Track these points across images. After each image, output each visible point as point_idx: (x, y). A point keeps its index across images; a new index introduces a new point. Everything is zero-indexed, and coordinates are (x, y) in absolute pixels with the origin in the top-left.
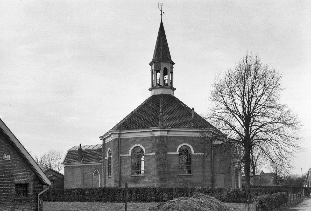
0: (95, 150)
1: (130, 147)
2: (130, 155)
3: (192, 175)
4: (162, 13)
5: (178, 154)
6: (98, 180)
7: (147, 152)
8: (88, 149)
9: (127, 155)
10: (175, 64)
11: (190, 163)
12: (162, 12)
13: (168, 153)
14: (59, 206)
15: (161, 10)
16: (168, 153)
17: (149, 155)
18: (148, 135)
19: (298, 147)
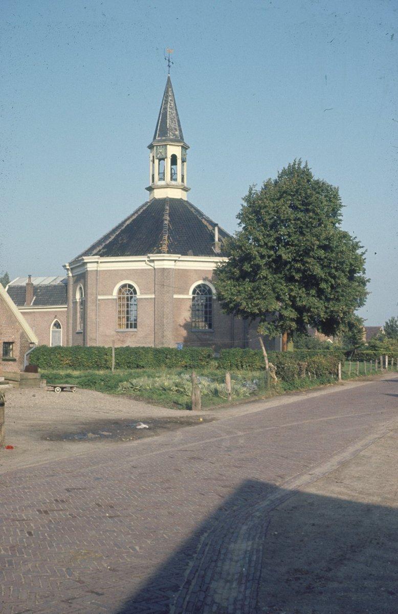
0: (55, 286)
1: (115, 284)
2: (115, 297)
3: (213, 331)
4: (171, 64)
5: (191, 297)
6: (59, 338)
7: (142, 294)
8: (42, 283)
9: (110, 297)
10: (189, 148)
11: (210, 312)
12: (170, 63)
13: (175, 296)
14: (118, 571)
15: (167, 59)
16: (175, 296)
17: (145, 299)
18: (142, 266)
19: (187, 449)
